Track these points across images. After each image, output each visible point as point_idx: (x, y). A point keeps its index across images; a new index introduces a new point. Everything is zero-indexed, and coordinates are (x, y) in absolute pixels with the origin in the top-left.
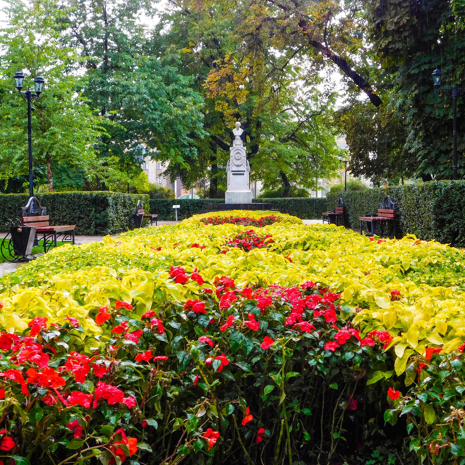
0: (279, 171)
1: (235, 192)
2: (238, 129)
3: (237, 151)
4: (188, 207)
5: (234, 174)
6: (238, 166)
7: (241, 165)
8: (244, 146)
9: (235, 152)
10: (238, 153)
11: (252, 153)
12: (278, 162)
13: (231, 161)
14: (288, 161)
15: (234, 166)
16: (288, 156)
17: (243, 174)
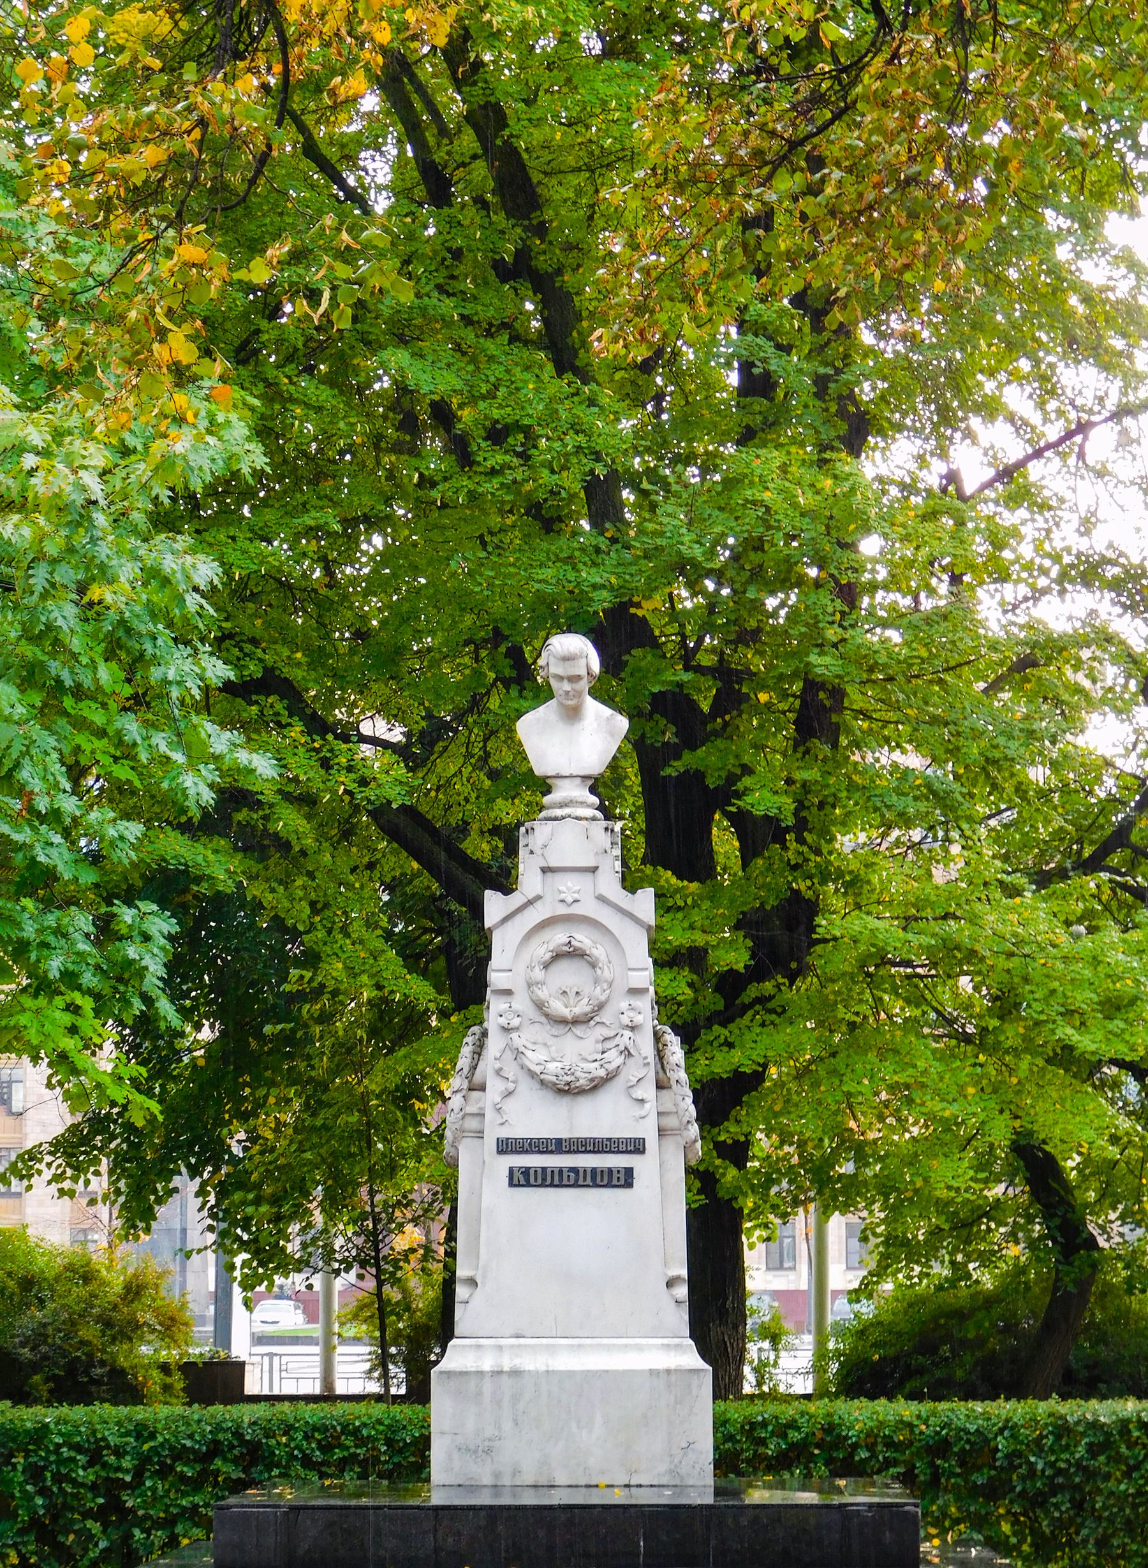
0: (1001, 1133)
1: (531, 1363)
2: (573, 714)
3: (558, 937)
4: (111, 1488)
5: (521, 1179)
6: (567, 1090)
7: (597, 1085)
8: (630, 883)
9: (541, 949)
10: (571, 953)
11: (757, 973)
12: (994, 1049)
13: (495, 1044)
14: (1087, 1043)
15: (527, 1091)
16: (1083, 998)
17: (627, 1179)
